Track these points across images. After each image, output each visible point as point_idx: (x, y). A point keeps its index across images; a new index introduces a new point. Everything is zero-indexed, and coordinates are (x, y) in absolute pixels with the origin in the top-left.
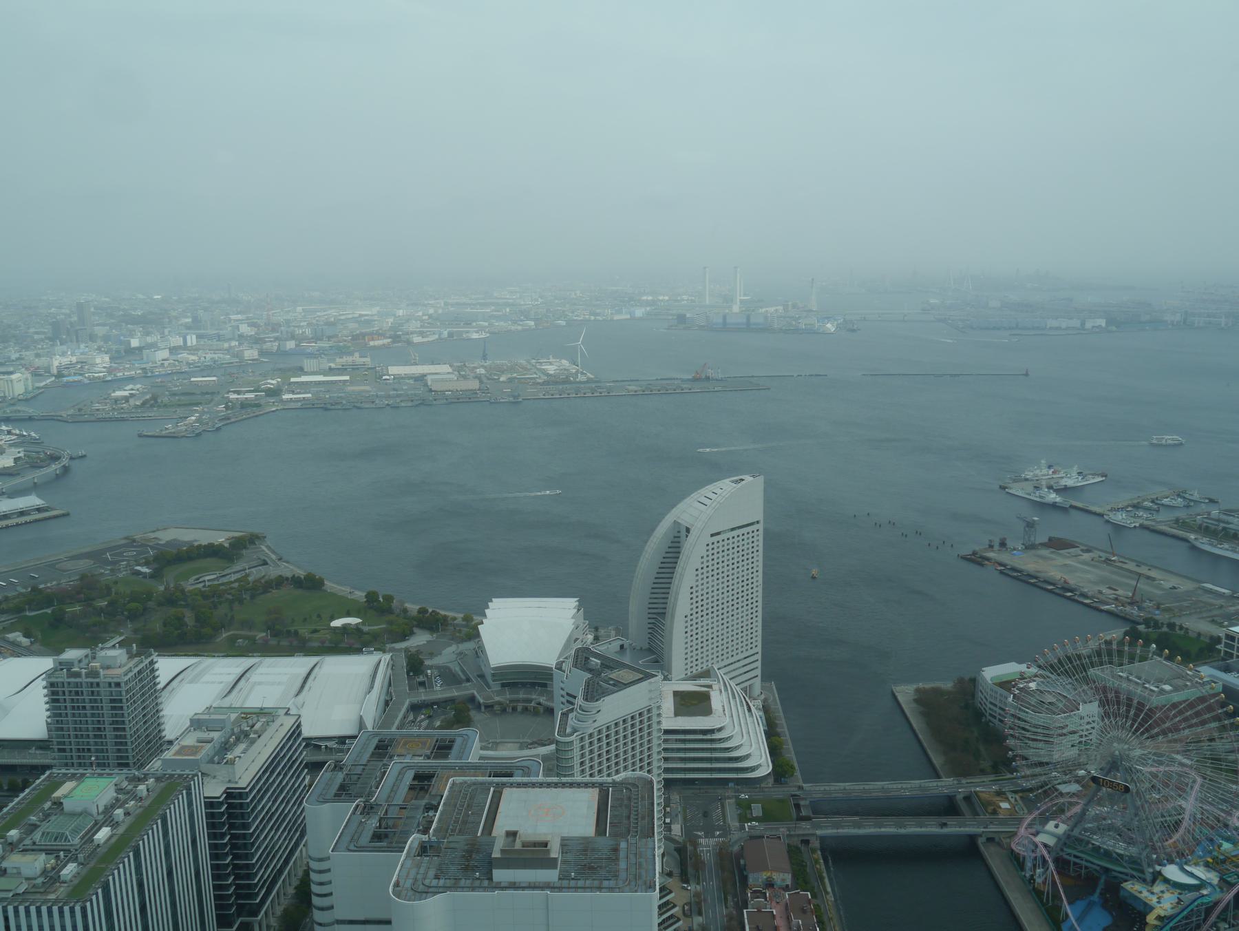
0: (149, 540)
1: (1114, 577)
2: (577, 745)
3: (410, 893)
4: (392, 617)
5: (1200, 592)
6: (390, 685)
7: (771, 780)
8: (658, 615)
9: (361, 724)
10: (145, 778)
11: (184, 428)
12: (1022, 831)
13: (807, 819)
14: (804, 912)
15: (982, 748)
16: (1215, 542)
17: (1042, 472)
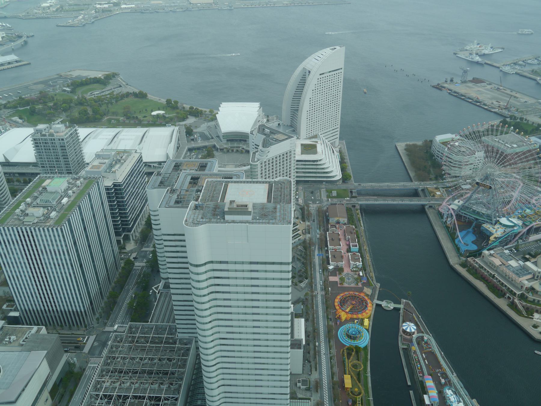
0: (68, 75)
1: (500, 96)
2: (259, 166)
3: (192, 224)
4: (178, 111)
5: (537, 104)
6: (179, 140)
7: (341, 181)
8: (295, 111)
9: (168, 157)
12: (444, 203)
14: (351, 233)
15: (431, 169)
17: (474, 47)
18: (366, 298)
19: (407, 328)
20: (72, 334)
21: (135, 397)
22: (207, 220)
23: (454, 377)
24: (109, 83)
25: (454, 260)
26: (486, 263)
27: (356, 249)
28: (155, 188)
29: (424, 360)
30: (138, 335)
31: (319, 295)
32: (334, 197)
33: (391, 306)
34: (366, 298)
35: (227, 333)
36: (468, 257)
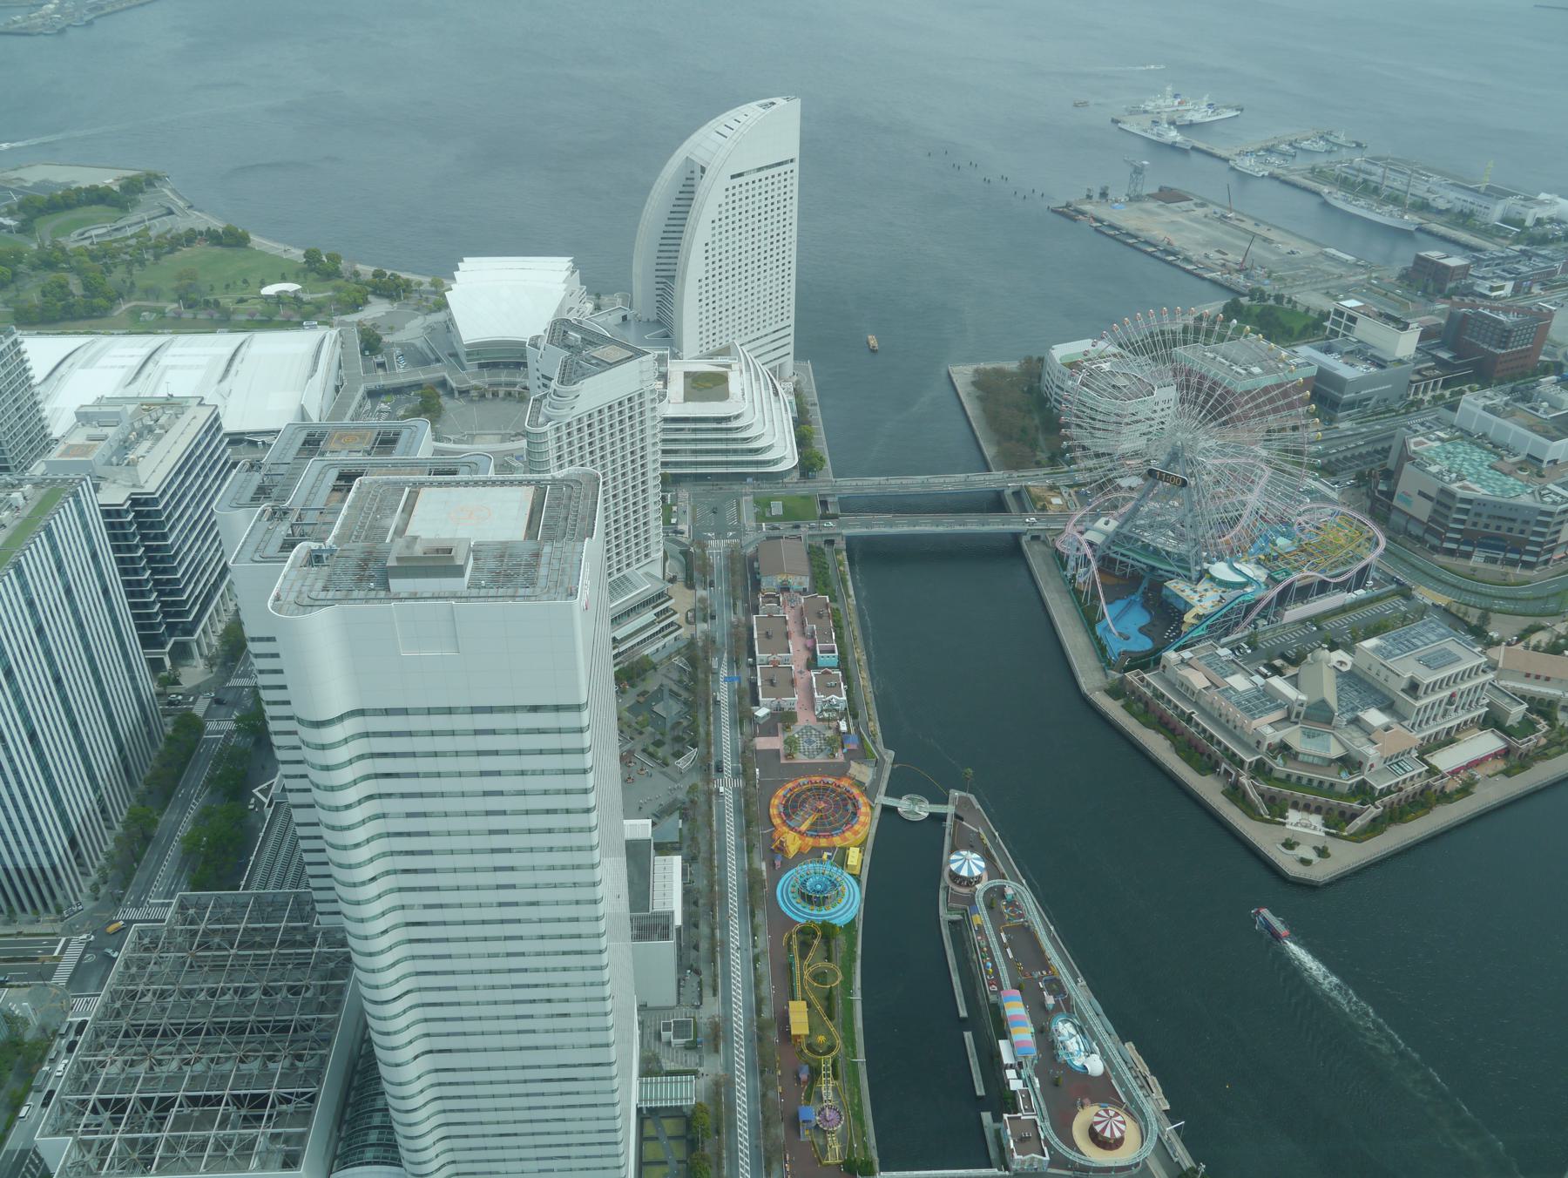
0: (10, 181)
1: (1228, 239)
2: (552, 436)
4: (339, 282)
5: (1320, 258)
7: (796, 474)
9: (303, 414)
10: (20, 484)
11: (39, 21)
12: (1070, 528)
13: (834, 517)
14: (820, 616)
15: (1041, 437)
16: (1350, 197)
17: (1165, 103)
18: (855, 791)
19: (960, 868)
20: (19, 934)
21: (194, 1101)
22: (339, 595)
23: (1079, 991)
24: (136, 203)
25: (1091, 679)
26: (1171, 685)
27: (833, 659)
28: (240, 506)
29: (1003, 947)
30: (203, 926)
31: (726, 788)
32: (777, 518)
33: (916, 808)
34: (855, 791)
35: (426, 907)
36: (1127, 669)
